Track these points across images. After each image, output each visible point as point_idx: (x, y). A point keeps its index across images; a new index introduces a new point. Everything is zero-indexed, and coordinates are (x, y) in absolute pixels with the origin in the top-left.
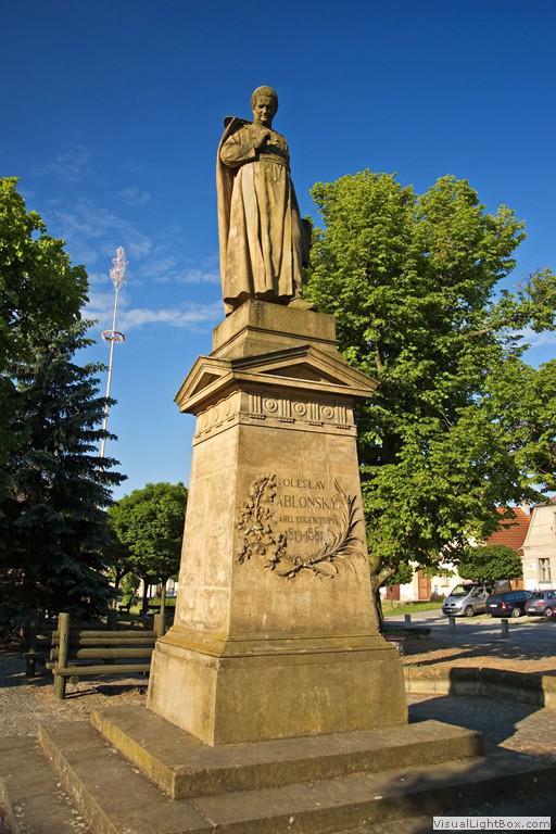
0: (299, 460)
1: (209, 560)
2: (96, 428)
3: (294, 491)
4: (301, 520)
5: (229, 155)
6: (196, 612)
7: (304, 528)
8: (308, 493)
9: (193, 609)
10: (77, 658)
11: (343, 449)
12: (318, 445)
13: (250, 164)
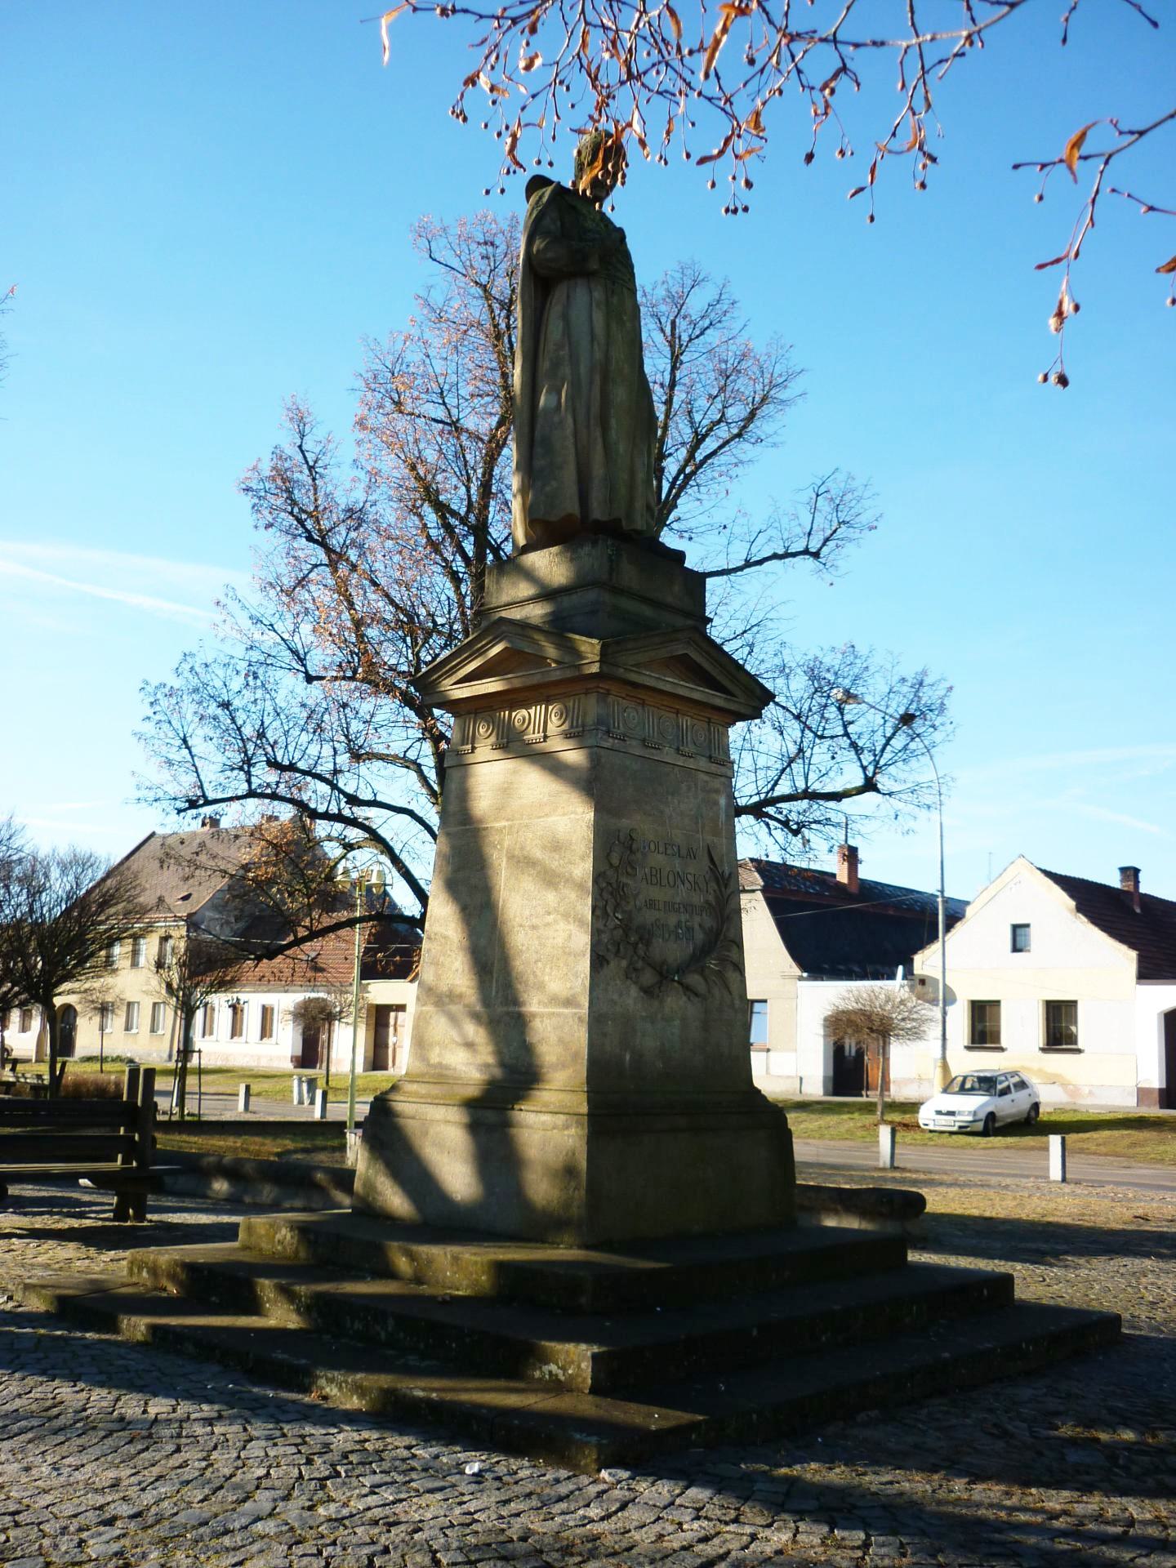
1: (336, 1458)
4: (670, 907)
7: (672, 920)
10: (205, 1196)
12: (689, 789)
13: (380, 831)
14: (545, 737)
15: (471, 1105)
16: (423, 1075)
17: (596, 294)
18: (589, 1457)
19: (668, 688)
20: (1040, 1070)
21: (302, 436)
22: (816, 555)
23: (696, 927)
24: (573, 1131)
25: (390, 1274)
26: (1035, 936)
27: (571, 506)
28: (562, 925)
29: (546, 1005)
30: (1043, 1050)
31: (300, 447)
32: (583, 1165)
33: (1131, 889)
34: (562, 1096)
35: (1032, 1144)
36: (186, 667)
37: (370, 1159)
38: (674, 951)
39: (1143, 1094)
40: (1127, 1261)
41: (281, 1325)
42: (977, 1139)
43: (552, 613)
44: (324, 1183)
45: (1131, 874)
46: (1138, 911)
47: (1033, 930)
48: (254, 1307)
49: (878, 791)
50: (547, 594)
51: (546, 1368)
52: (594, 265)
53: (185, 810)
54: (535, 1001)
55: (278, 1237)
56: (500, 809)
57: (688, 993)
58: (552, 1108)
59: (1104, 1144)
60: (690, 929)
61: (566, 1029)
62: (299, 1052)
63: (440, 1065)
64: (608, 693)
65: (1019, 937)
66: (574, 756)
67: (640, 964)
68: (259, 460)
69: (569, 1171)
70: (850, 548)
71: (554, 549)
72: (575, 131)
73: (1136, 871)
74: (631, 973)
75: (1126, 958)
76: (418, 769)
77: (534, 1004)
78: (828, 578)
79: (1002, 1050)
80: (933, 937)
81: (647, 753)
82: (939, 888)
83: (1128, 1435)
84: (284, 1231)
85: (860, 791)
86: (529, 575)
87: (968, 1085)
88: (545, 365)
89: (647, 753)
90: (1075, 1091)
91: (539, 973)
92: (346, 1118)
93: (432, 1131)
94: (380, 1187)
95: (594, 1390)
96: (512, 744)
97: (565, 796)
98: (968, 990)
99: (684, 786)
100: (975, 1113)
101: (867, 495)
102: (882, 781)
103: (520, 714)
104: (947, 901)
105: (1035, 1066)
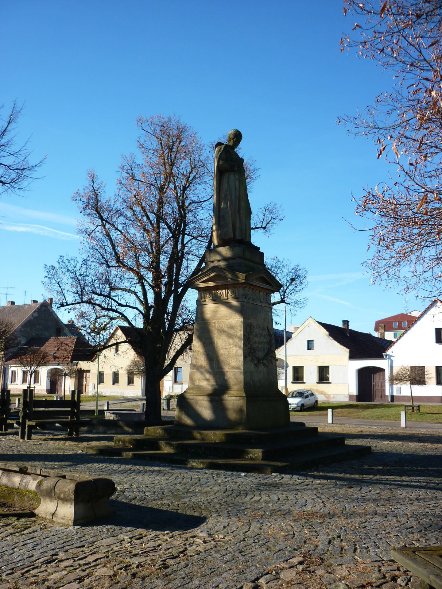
7: (260, 346)
14: (228, 298)
15: (209, 395)
16: (194, 388)
17: (237, 177)
18: (269, 470)
19: (259, 285)
20: (317, 390)
21: (93, 182)
22: (265, 228)
24: (242, 401)
25: (195, 439)
26: (315, 344)
27: (231, 236)
28: (234, 348)
29: (230, 369)
30: (318, 383)
31: (93, 186)
32: (245, 409)
33: (346, 328)
34: (237, 392)
35: (317, 414)
36: (61, 260)
37: (179, 411)
38: (260, 354)
39: (351, 397)
40: (364, 440)
41: (169, 452)
42: (298, 413)
43: (227, 265)
44: (122, 425)
45: (346, 322)
46: (348, 335)
47: (314, 342)
48: (159, 448)
49: (285, 303)
50: (224, 259)
51: (249, 455)
52: (236, 169)
53: (60, 307)
54: (227, 368)
55: (157, 432)
56: (214, 317)
58: (235, 395)
59: (340, 413)
60: (264, 349)
61: (237, 375)
62: (49, 388)
63: (199, 385)
64: (245, 287)
65: (310, 345)
66: (235, 303)
67: (254, 358)
68: (79, 190)
69: (241, 411)
70: (275, 226)
71: (227, 247)
73: (348, 322)
74: (252, 360)
75: (345, 352)
76: (135, 293)
77: (226, 369)
78: (267, 235)
79: (304, 383)
80: (283, 344)
82: (284, 328)
83: (380, 468)
84: (159, 430)
85: (279, 302)
86: (219, 253)
87: (294, 395)
88: (223, 196)
90: (328, 396)
91: (228, 360)
92: (94, 408)
93: (199, 403)
94: (183, 418)
95: (262, 459)
96: (217, 300)
97: (234, 314)
98: (292, 362)
99: (262, 311)
100: (297, 404)
101: (280, 210)
102: (287, 300)
103: (219, 292)
104: (287, 332)
105: (315, 388)
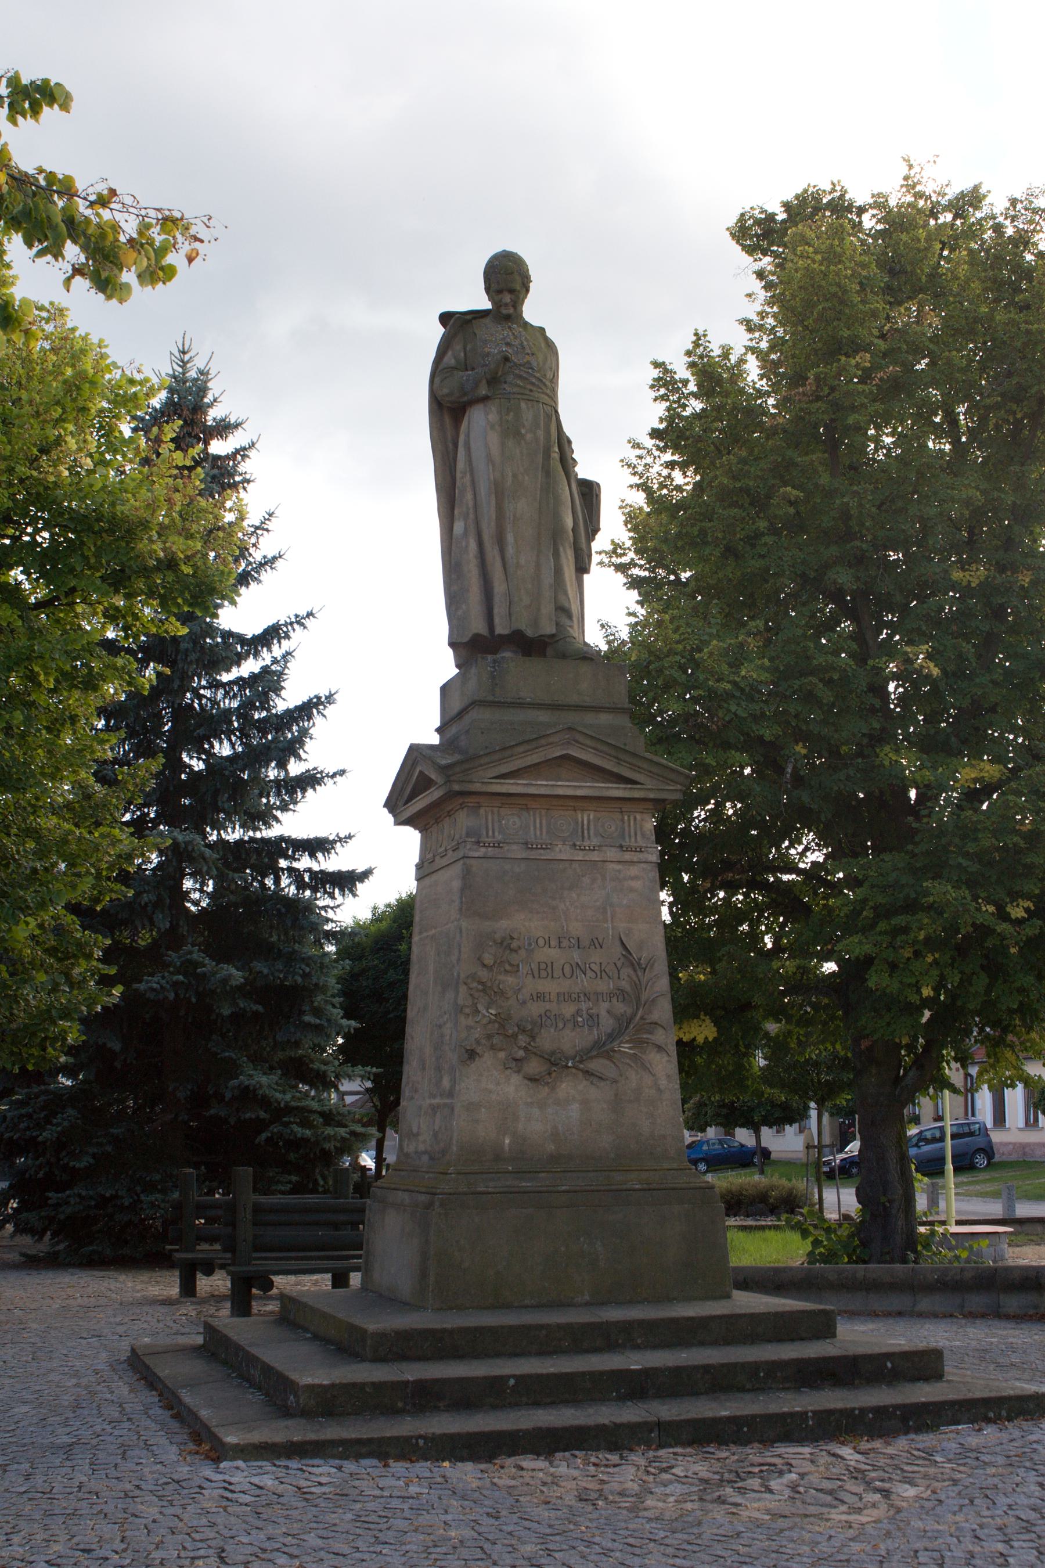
0: (562, 906)
2: (295, 768)
3: (553, 953)
4: (565, 997)
5: (446, 391)
6: (421, 1138)
7: (568, 1010)
8: (576, 956)
9: (418, 1134)
11: (637, 884)
19: (543, 791)
23: (603, 1013)
57: (592, 1078)
64: (479, 806)
72: (274, 559)
81: (533, 854)
89: (533, 854)
